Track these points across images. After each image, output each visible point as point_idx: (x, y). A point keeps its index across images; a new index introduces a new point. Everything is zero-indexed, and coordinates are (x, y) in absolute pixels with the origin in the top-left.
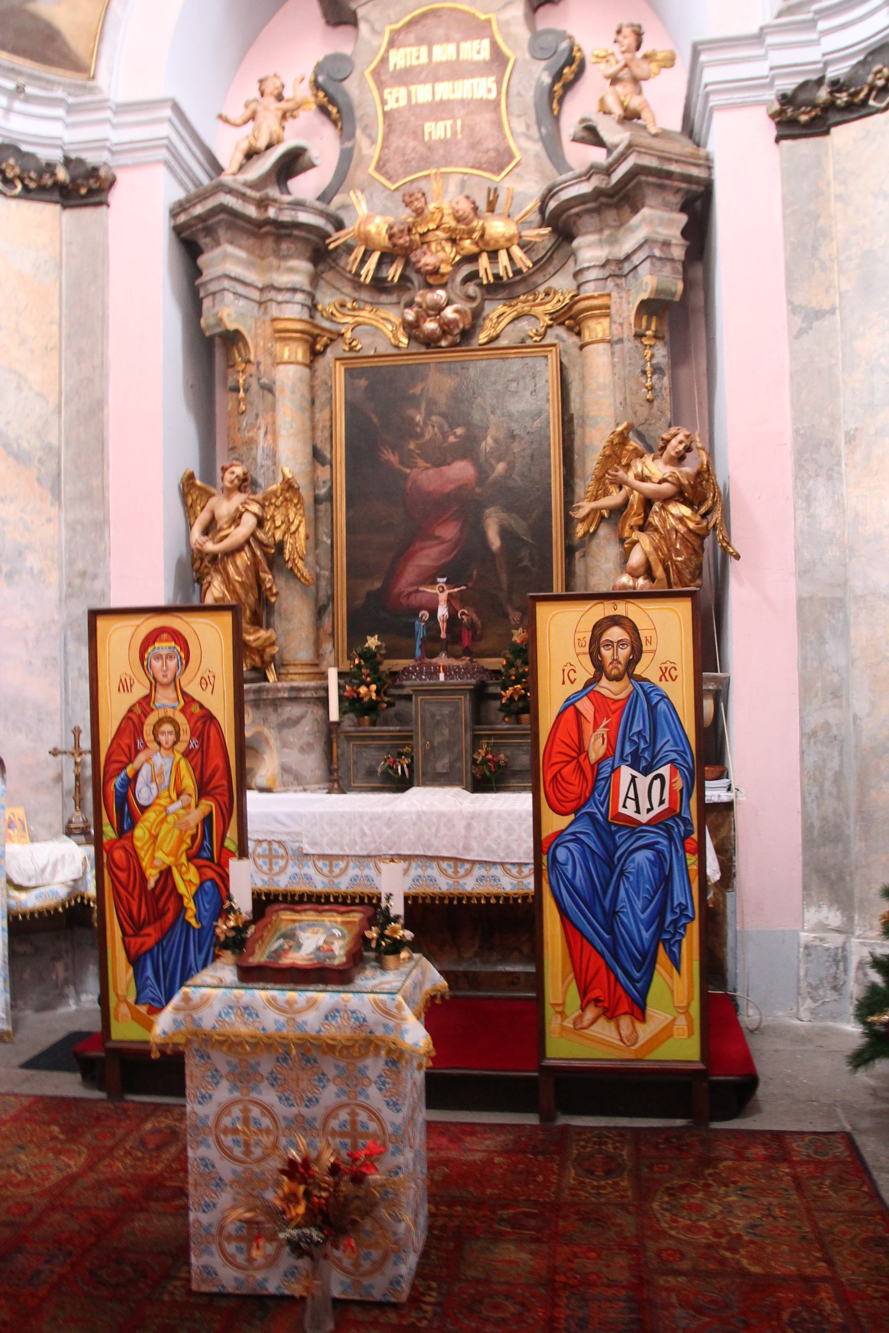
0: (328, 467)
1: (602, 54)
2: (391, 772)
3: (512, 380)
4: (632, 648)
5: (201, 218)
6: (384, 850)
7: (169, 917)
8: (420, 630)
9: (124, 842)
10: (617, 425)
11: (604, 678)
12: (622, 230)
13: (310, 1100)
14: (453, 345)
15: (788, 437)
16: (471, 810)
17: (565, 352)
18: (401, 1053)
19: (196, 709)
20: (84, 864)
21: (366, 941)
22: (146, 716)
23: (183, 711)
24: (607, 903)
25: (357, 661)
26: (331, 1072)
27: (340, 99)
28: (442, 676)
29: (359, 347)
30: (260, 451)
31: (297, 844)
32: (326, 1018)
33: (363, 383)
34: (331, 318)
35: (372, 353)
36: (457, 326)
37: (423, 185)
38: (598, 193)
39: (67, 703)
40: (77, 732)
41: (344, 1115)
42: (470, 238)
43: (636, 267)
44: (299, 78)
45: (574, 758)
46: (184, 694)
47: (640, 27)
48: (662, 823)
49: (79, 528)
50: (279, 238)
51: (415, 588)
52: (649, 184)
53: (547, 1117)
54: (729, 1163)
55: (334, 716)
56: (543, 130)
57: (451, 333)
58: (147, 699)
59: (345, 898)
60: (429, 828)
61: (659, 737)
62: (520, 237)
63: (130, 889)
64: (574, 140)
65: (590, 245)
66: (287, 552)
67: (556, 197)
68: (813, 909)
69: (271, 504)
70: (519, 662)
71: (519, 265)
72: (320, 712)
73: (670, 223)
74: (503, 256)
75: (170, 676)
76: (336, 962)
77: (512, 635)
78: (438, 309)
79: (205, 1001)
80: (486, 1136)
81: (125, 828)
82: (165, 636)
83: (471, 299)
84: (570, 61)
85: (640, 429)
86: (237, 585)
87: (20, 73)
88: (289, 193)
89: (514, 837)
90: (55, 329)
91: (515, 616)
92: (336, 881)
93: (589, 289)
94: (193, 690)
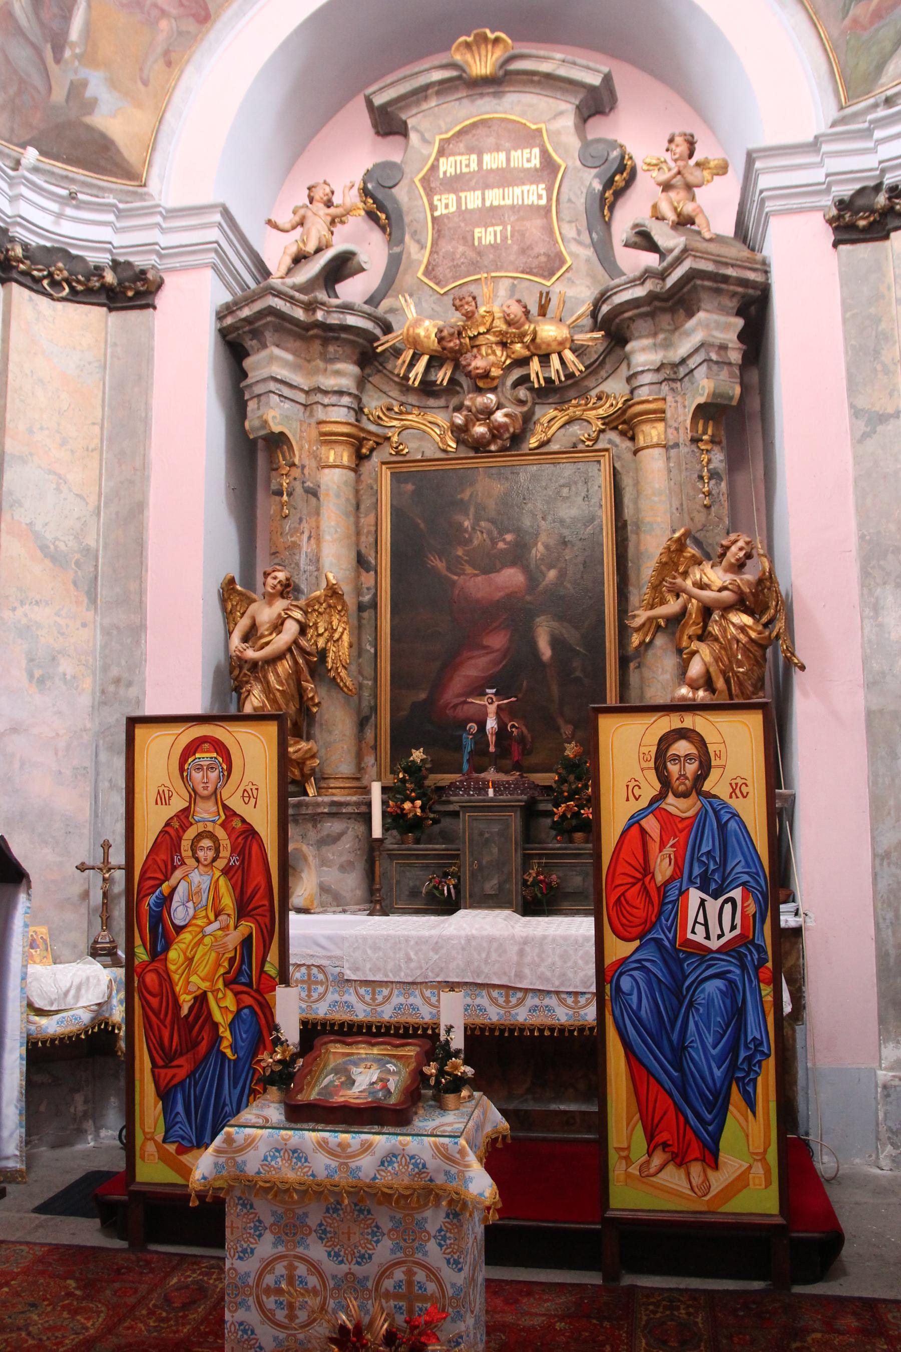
0: (372, 573)
1: (654, 162)
2: (437, 893)
3: (563, 486)
4: (701, 762)
5: (247, 320)
6: (431, 977)
7: (203, 1047)
8: (468, 744)
9: (156, 965)
10: (674, 531)
11: (670, 794)
12: (677, 334)
13: (362, 1257)
14: (503, 449)
15: (853, 543)
16: (525, 935)
17: (619, 457)
18: (465, 1205)
19: (237, 824)
20: (110, 987)
21: (425, 1078)
22: (184, 831)
23: (223, 825)
24: (675, 1037)
25: (401, 776)
26: (386, 1224)
27: (389, 206)
28: (491, 792)
29: (406, 450)
30: (303, 556)
31: (338, 969)
32: (382, 1163)
33: (410, 487)
34: (377, 421)
35: (419, 457)
36: (508, 430)
37: (472, 288)
38: (652, 297)
39: (96, 816)
40: (106, 846)
41: (399, 1274)
42: (522, 342)
43: (692, 371)
44: (349, 185)
45: (639, 880)
46: (225, 807)
47: (692, 136)
48: (733, 950)
49: (115, 632)
50: (326, 342)
51: (462, 699)
52: (703, 287)
53: (611, 1277)
54: (819, 1335)
55: (377, 832)
56: (594, 235)
57: (500, 438)
58: (186, 812)
59: (388, 1028)
60: (479, 954)
61: (730, 855)
62: (573, 341)
63: (162, 1016)
64: (627, 245)
65: (643, 349)
66: (330, 660)
67: (609, 302)
68: (891, 1045)
69: (314, 610)
70: (572, 778)
71: (572, 368)
72: (360, 828)
73: (727, 327)
74: (555, 360)
75: (211, 788)
76: (393, 1100)
77: (565, 749)
78: (488, 413)
79: (250, 1143)
80: (546, 1297)
81: (158, 953)
82: (206, 746)
83: (521, 402)
84: (621, 169)
85: (697, 535)
86: (278, 694)
87: (72, 181)
88: (337, 297)
89: (570, 964)
90: (97, 429)
91: (567, 730)
92: (379, 1009)
93: (643, 393)
94: (236, 803)
